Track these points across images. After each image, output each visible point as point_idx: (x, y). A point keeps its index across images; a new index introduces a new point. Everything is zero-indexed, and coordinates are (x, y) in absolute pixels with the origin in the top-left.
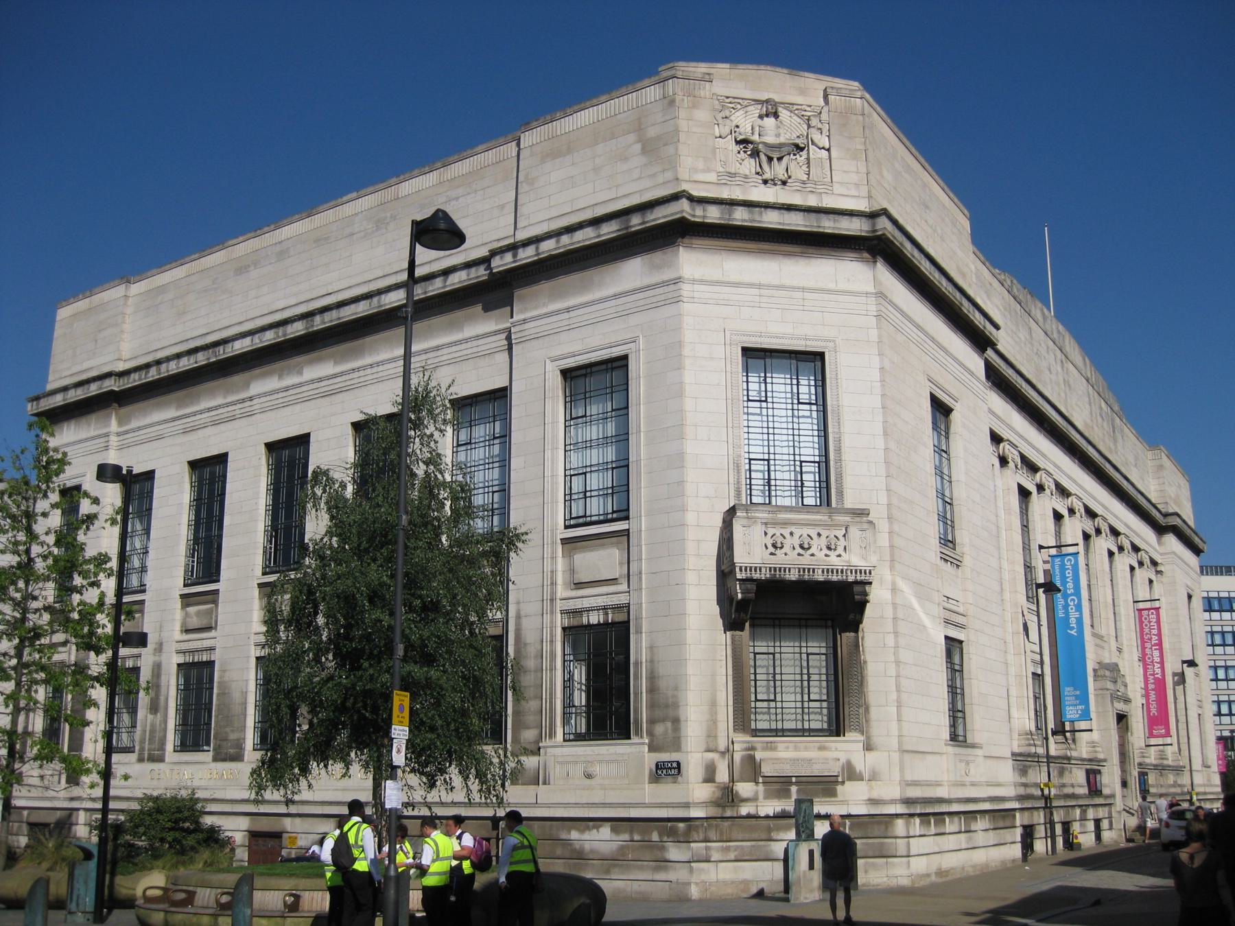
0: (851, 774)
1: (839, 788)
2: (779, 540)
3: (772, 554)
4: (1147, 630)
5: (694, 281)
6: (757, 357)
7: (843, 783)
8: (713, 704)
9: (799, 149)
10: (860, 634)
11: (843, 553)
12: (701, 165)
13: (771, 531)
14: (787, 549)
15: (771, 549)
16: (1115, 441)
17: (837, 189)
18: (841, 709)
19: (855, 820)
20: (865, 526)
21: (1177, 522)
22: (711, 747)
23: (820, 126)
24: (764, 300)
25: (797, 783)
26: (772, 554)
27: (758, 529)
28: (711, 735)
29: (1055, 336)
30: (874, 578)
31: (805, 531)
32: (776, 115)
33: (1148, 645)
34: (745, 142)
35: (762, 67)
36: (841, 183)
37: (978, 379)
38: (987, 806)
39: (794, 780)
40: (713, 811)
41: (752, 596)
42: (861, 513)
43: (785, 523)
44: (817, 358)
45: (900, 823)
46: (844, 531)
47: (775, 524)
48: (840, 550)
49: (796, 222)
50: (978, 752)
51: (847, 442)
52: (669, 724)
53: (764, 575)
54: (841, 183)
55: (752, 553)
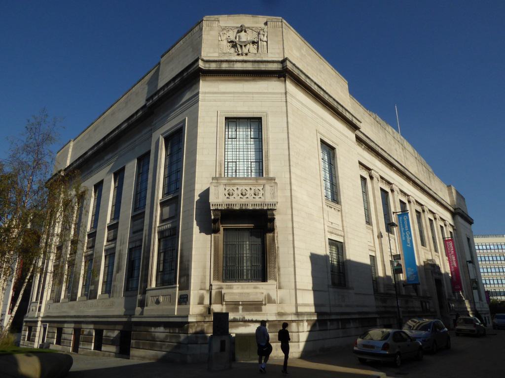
0: (270, 300)
1: (263, 307)
2: (231, 192)
3: (228, 198)
4: (449, 249)
5: (205, 93)
6: (232, 121)
7: (265, 304)
8: (205, 268)
9: (253, 43)
10: (276, 235)
11: (262, 197)
12: (212, 50)
13: (227, 188)
14: (235, 195)
15: (227, 196)
16: (430, 181)
17: (270, 55)
18: (262, 271)
19: (271, 323)
20: (273, 184)
21: (460, 211)
22: (203, 288)
23: (264, 33)
24: (235, 98)
25: (242, 305)
26: (228, 198)
27: (222, 187)
28: (203, 282)
29: (399, 139)
30: (278, 207)
31: (244, 188)
32: (245, 32)
33: (450, 255)
34: (231, 42)
35: (241, 15)
36: (272, 53)
37: (353, 142)
38: (357, 316)
39: (241, 303)
40: (199, 319)
41: (219, 217)
42: (273, 179)
43: (234, 184)
44: (259, 120)
45: (294, 324)
46: (262, 187)
47: (229, 185)
48: (260, 195)
49: (249, 67)
50: (351, 291)
51: (271, 153)
52: (185, 277)
53: (224, 207)
54: (272, 53)
55: (218, 199)
